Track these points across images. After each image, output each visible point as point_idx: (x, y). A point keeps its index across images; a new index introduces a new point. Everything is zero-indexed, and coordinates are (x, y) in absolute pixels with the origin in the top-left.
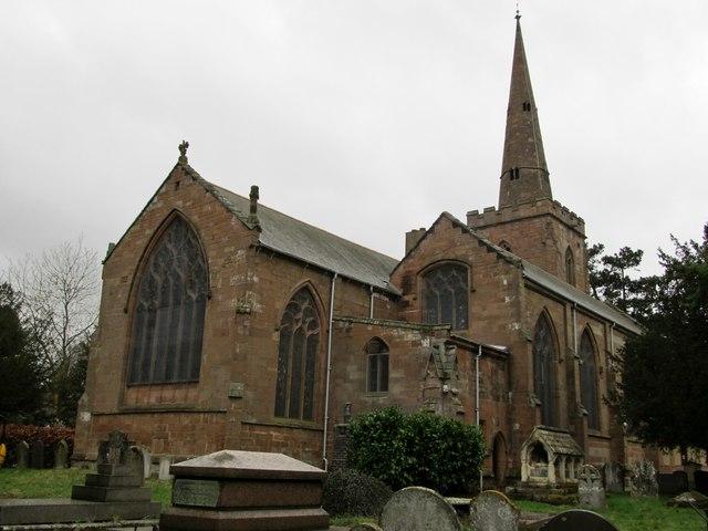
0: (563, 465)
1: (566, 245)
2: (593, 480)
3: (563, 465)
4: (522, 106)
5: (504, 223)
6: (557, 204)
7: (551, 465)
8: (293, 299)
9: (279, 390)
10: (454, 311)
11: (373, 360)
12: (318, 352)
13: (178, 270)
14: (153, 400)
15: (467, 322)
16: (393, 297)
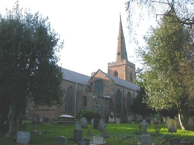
1: (130, 71)
4: (122, 38)
10: (101, 89)
16: (89, 87)
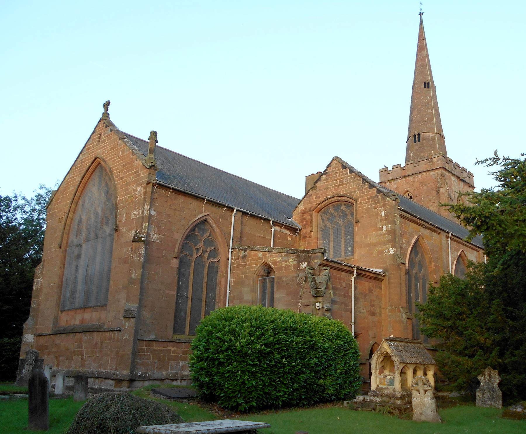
0: (409, 374)
3: (409, 374)
4: (424, 84)
7: (397, 373)
10: (343, 240)
11: (263, 282)
15: (353, 248)
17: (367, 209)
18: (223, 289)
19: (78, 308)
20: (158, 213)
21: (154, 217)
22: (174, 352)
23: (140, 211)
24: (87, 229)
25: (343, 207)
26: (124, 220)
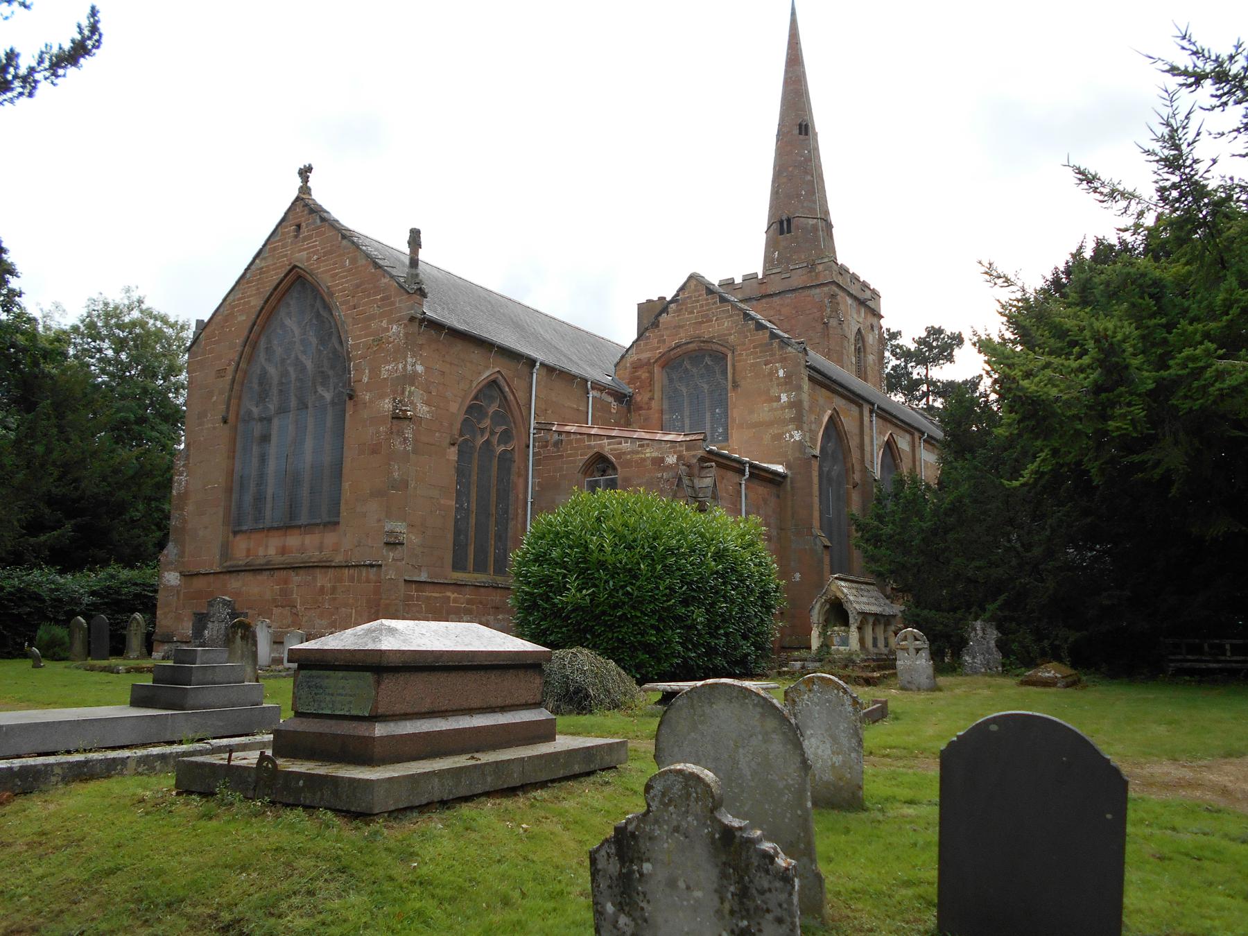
2: (918, 650)
5: (770, 296)
6: (843, 270)
7: (853, 630)
8: (476, 398)
9: (458, 532)
10: (708, 415)
12: (514, 477)
13: (303, 358)
14: (272, 551)
15: (726, 430)
16: (620, 397)
17: (752, 365)
18: (521, 496)
19: (270, 529)
20: (427, 368)
21: (421, 376)
22: (455, 601)
23: (400, 366)
24: (281, 391)
25: (707, 360)
26: (365, 379)
